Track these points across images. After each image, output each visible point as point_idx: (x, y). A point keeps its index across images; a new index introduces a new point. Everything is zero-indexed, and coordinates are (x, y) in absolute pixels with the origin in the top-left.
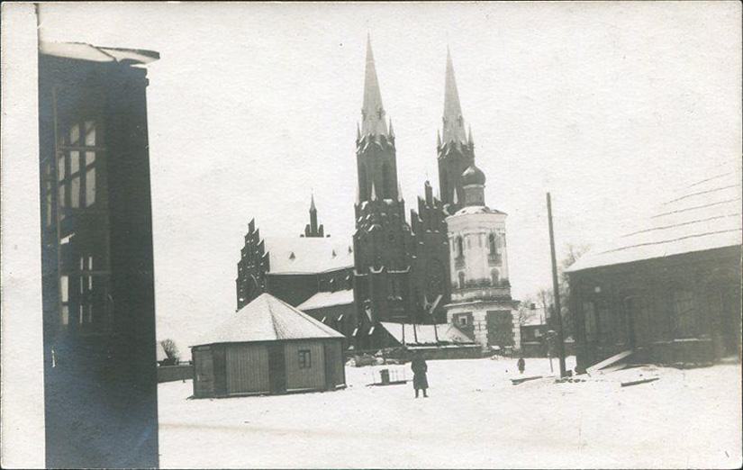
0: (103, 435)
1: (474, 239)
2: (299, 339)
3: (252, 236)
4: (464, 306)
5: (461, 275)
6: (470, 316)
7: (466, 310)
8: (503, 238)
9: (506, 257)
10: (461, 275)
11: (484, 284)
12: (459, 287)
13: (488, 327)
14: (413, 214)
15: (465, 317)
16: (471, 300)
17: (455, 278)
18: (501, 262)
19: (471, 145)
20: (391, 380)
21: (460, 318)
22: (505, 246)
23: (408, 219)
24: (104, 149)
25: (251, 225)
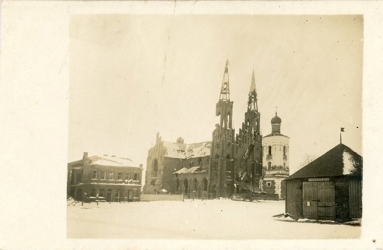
0: (92, 6)
1: (278, 148)
2: (362, 55)
4: (271, 177)
5: (270, 163)
6: (273, 182)
7: (272, 179)
8: (288, 148)
9: (289, 159)
10: (270, 163)
11: (280, 168)
12: (267, 168)
13: (281, 188)
15: (271, 182)
16: (275, 175)
17: (265, 164)
18: (287, 159)
19: (234, 130)
20: (309, 181)
21: (267, 183)
22: (289, 152)
23: (235, 136)
24: (102, 188)
25: (158, 134)
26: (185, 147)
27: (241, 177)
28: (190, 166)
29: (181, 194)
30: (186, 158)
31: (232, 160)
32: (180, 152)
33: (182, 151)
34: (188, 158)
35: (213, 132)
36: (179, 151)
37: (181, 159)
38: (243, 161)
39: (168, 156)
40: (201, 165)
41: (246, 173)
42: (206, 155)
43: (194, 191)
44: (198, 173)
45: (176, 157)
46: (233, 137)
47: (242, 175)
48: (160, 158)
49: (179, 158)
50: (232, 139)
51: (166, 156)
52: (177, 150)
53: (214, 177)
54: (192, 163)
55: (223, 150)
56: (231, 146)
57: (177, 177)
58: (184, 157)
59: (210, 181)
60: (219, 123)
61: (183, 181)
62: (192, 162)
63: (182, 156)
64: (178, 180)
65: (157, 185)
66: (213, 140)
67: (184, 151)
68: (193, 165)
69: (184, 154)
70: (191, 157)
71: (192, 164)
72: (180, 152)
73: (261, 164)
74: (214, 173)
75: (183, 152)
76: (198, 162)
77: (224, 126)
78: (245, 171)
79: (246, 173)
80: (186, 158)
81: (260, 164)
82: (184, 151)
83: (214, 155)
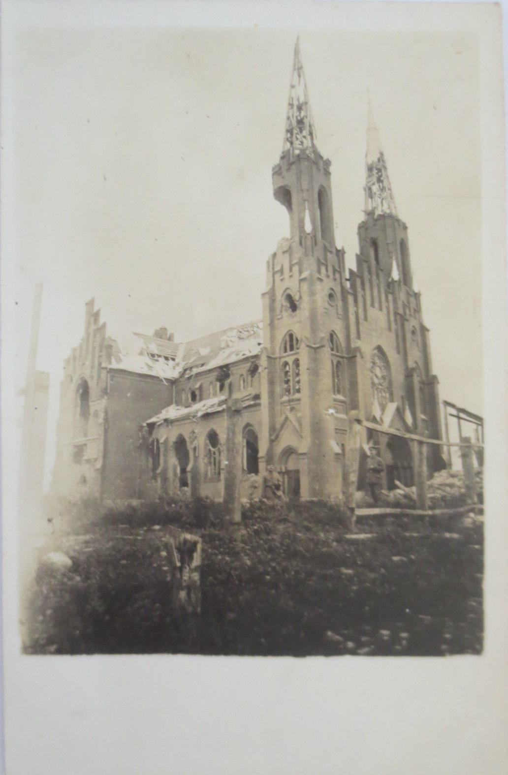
14: (351, 272)
26: (176, 347)
28: (194, 398)
29: (411, 369)
32: (162, 360)
33: (167, 359)
35: (267, 259)
36: (159, 356)
40: (231, 392)
51: (150, 367)
53: (287, 419)
54: (197, 389)
55: (313, 318)
59: (270, 435)
61: (171, 443)
62: (197, 386)
63: (166, 371)
65: (88, 461)
66: (270, 287)
68: (201, 395)
71: (197, 393)
72: (160, 359)
74: (282, 403)
75: (171, 363)
76: (218, 384)
78: (381, 402)
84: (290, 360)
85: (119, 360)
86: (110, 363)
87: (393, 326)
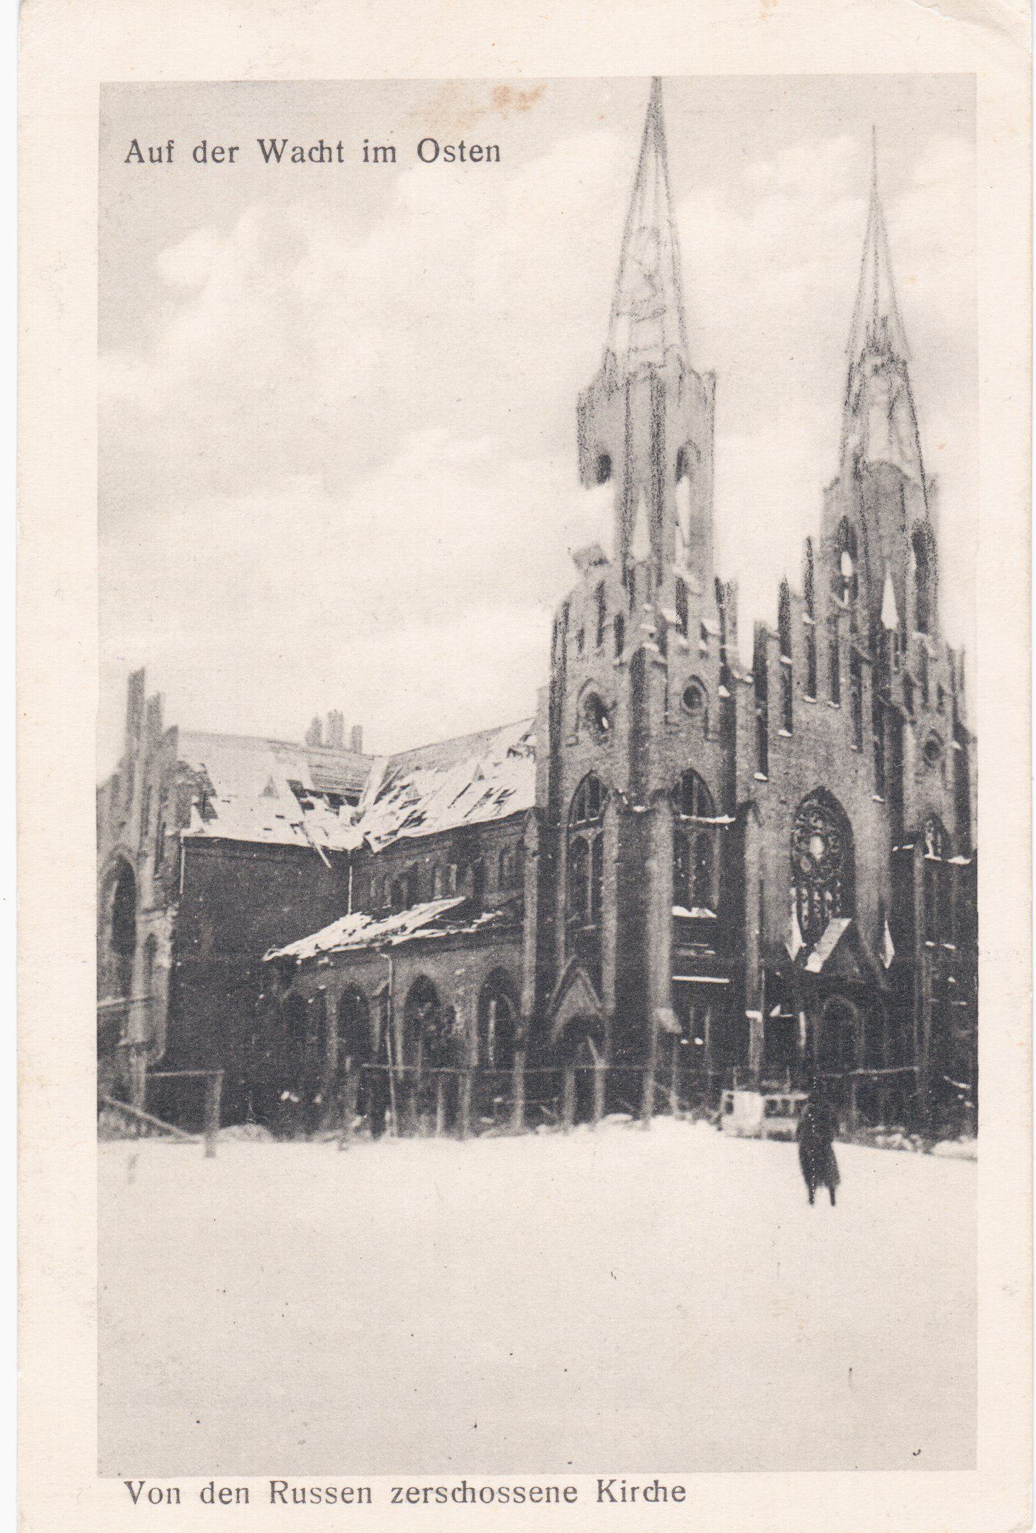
3: (135, 1502)
27: (804, 954)
30: (366, 845)
31: (726, 819)
32: (321, 804)
34: (378, 838)
37: (325, 849)
38: (817, 835)
39: (215, 830)
41: (845, 923)
42: (508, 809)
43: (839, 1076)
44: (448, 938)
45: (283, 835)
46: (723, 640)
47: (812, 936)
48: (150, 849)
49: (305, 844)
50: (715, 654)
51: (202, 831)
52: (298, 791)
56: (715, 709)
57: (286, 981)
58: (349, 840)
60: (606, 535)
64: (297, 1000)
67: (354, 801)
69: (356, 820)
70: (400, 834)
73: (967, 861)
75: (347, 810)
77: (641, 549)
79: (845, 923)
80: (366, 845)
81: (959, 860)
82: (354, 801)
83: (570, 785)
84: (589, 834)
85: (207, 813)
86: (187, 824)
87: (869, 736)
